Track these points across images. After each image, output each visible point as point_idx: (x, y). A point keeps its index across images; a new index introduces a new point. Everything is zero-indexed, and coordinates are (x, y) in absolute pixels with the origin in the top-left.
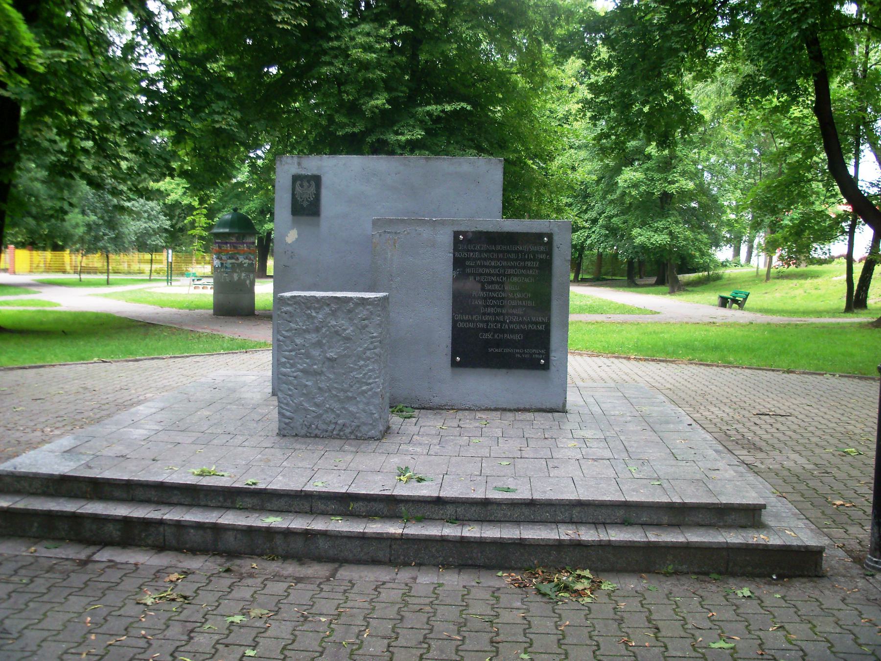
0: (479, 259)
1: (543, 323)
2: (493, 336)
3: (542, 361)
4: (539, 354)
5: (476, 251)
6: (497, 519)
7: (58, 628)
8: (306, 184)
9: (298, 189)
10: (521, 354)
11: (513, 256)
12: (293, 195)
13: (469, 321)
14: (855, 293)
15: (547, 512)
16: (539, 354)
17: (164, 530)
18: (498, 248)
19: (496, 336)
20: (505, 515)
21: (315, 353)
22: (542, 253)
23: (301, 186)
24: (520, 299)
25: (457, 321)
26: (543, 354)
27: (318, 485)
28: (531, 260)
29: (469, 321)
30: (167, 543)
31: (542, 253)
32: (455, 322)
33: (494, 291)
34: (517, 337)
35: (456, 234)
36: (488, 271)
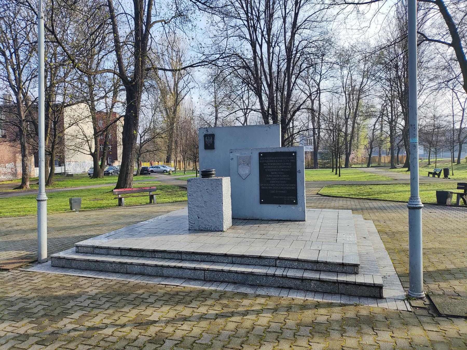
0: (269, 163)
1: (294, 186)
2: (275, 192)
3: (294, 201)
4: (293, 198)
5: (267, 160)
6: (247, 263)
7: (69, 308)
8: (209, 138)
9: (206, 140)
10: (286, 198)
11: (281, 161)
12: (205, 142)
13: (266, 186)
14: (144, 31)
15: (266, 261)
16: (293, 198)
17: (127, 267)
18: (275, 158)
19: (276, 192)
20: (250, 262)
21: (200, 199)
22: (292, 159)
23: (208, 138)
24: (285, 177)
25: (261, 186)
26: (294, 198)
27: (303, 256)
28: (288, 162)
29: (266, 186)
30: (128, 271)
31: (292, 159)
32: (260, 187)
33: (275, 174)
34: (284, 192)
35: (260, 153)
36: (272, 167)
